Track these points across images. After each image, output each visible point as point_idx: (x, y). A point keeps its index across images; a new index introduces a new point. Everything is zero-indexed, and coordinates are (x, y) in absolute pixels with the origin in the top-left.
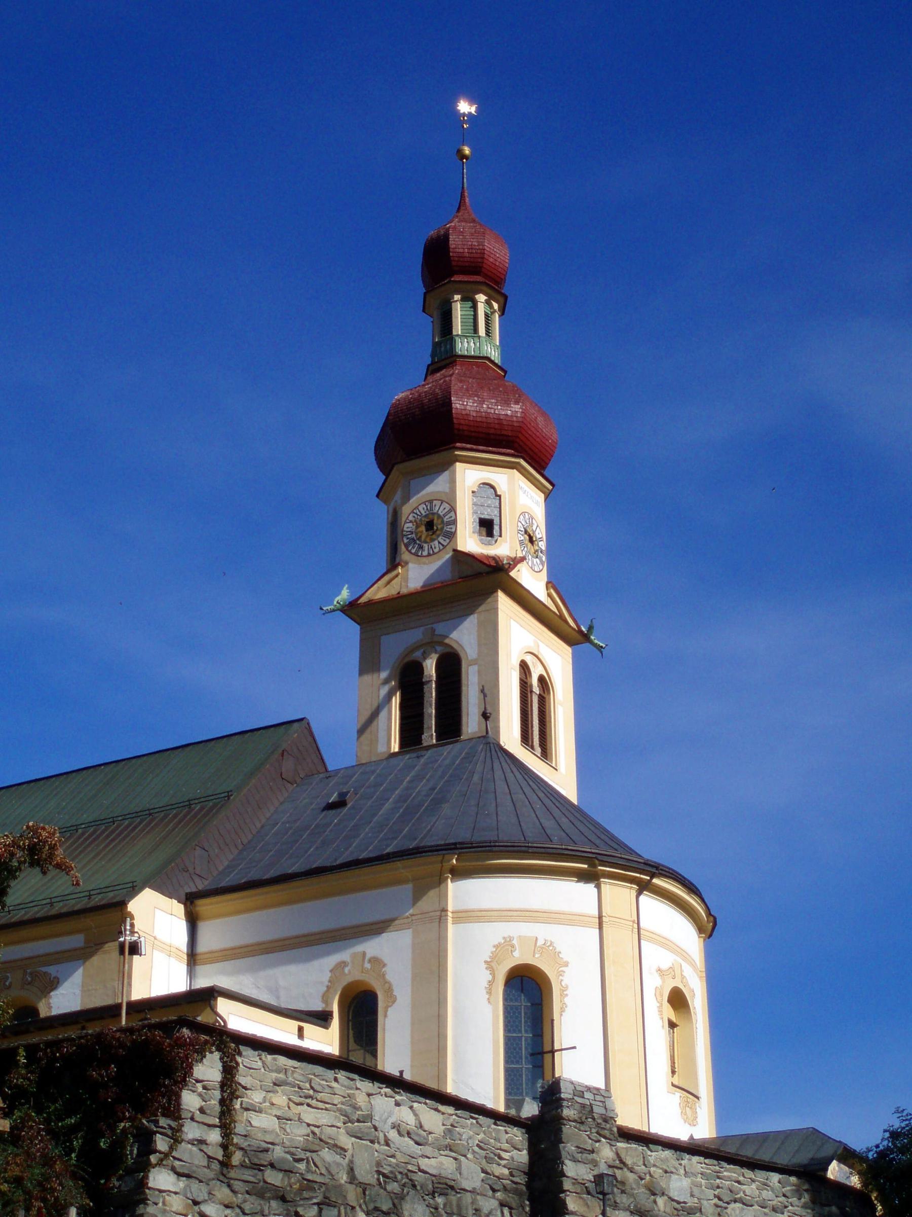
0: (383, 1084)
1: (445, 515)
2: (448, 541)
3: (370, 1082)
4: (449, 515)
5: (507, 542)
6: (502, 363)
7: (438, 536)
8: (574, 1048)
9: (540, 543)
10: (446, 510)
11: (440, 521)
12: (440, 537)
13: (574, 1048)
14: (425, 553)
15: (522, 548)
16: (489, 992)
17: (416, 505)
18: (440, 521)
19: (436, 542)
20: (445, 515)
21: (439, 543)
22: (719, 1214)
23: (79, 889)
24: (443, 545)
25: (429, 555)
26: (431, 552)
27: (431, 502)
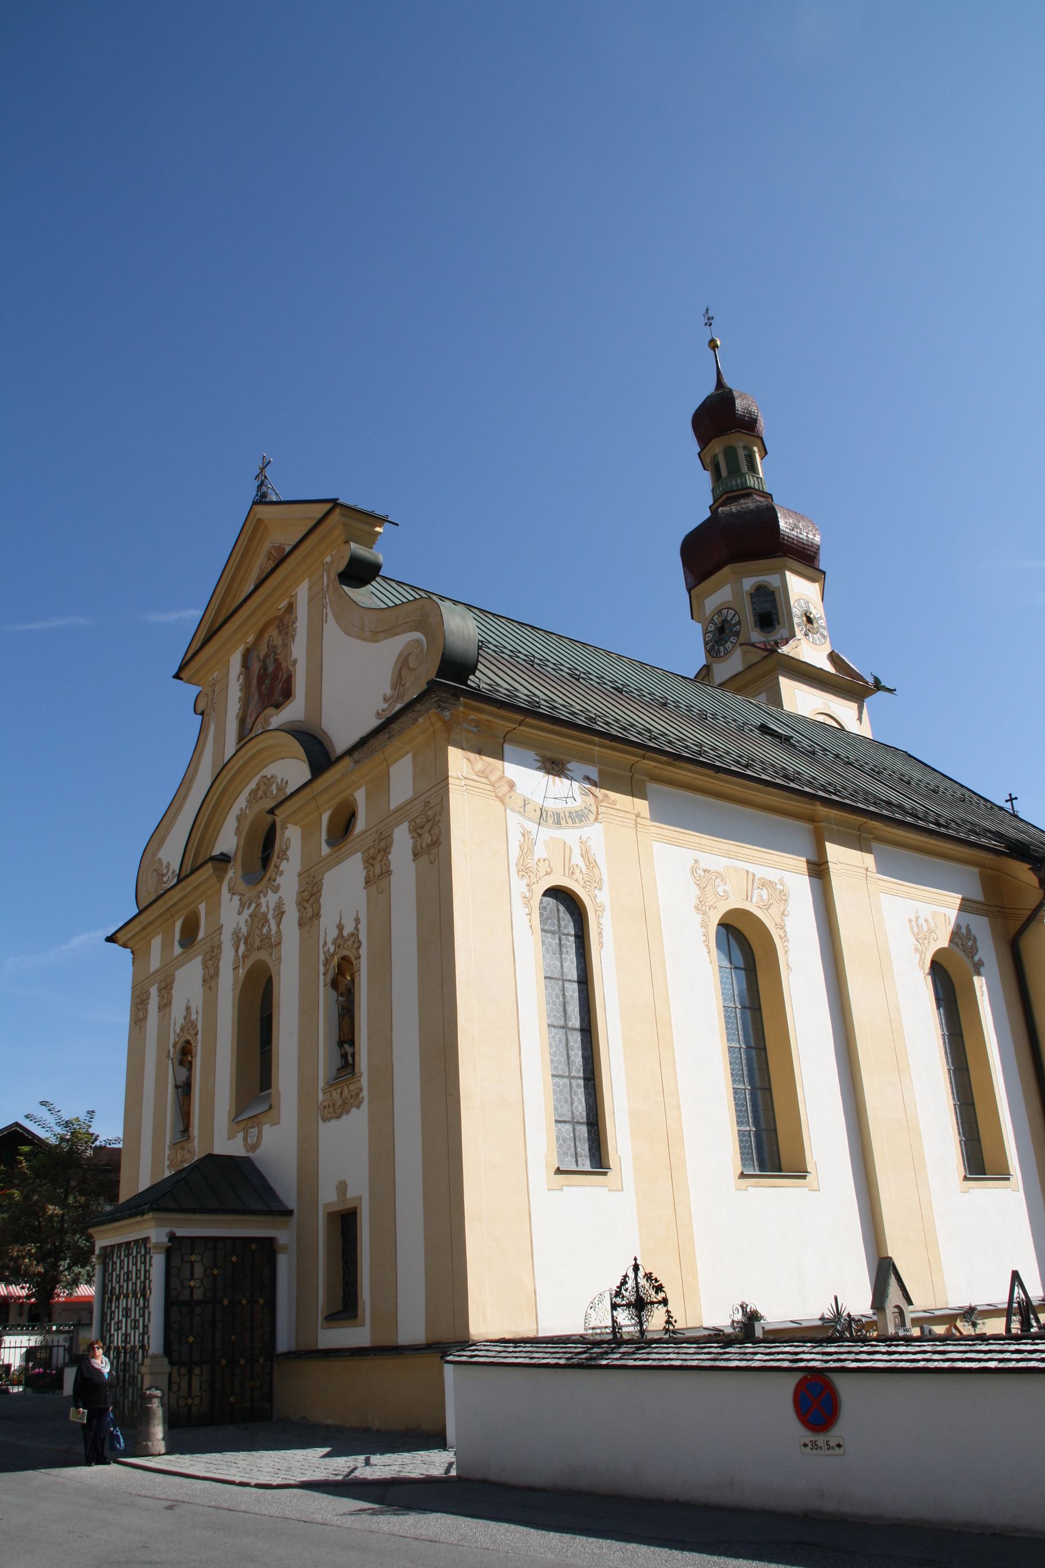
0: (953, 1066)
1: (731, 620)
2: (736, 638)
3: (415, 721)
4: (735, 618)
5: (785, 628)
6: (873, 736)
7: (730, 637)
8: (397, 525)
9: (822, 621)
10: (732, 615)
11: (729, 624)
12: (732, 638)
13: (397, 525)
14: (722, 654)
15: (800, 629)
16: (443, 601)
17: (711, 617)
18: (729, 624)
19: (729, 642)
20: (731, 620)
21: (731, 642)
22: (2, 1519)
23: (590, 806)
24: (733, 643)
25: (725, 654)
26: (726, 652)
27: (720, 611)
